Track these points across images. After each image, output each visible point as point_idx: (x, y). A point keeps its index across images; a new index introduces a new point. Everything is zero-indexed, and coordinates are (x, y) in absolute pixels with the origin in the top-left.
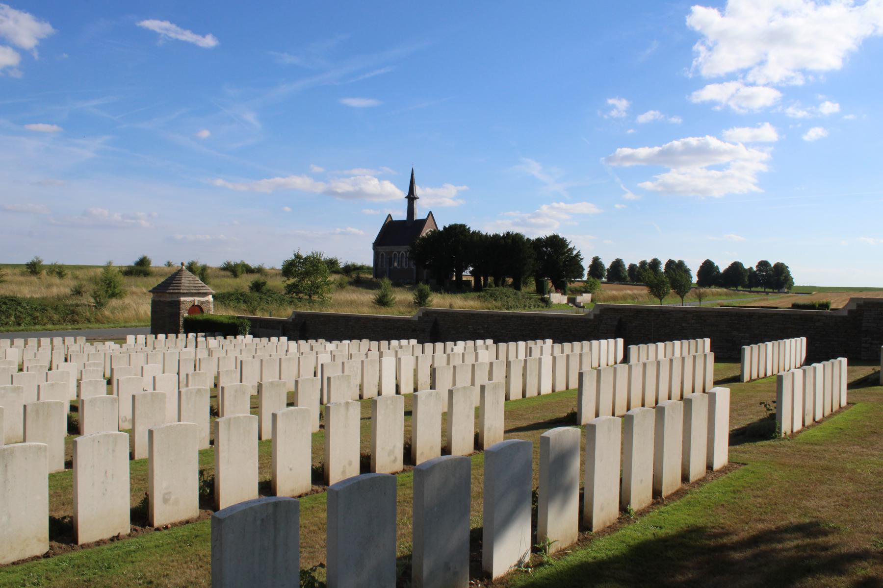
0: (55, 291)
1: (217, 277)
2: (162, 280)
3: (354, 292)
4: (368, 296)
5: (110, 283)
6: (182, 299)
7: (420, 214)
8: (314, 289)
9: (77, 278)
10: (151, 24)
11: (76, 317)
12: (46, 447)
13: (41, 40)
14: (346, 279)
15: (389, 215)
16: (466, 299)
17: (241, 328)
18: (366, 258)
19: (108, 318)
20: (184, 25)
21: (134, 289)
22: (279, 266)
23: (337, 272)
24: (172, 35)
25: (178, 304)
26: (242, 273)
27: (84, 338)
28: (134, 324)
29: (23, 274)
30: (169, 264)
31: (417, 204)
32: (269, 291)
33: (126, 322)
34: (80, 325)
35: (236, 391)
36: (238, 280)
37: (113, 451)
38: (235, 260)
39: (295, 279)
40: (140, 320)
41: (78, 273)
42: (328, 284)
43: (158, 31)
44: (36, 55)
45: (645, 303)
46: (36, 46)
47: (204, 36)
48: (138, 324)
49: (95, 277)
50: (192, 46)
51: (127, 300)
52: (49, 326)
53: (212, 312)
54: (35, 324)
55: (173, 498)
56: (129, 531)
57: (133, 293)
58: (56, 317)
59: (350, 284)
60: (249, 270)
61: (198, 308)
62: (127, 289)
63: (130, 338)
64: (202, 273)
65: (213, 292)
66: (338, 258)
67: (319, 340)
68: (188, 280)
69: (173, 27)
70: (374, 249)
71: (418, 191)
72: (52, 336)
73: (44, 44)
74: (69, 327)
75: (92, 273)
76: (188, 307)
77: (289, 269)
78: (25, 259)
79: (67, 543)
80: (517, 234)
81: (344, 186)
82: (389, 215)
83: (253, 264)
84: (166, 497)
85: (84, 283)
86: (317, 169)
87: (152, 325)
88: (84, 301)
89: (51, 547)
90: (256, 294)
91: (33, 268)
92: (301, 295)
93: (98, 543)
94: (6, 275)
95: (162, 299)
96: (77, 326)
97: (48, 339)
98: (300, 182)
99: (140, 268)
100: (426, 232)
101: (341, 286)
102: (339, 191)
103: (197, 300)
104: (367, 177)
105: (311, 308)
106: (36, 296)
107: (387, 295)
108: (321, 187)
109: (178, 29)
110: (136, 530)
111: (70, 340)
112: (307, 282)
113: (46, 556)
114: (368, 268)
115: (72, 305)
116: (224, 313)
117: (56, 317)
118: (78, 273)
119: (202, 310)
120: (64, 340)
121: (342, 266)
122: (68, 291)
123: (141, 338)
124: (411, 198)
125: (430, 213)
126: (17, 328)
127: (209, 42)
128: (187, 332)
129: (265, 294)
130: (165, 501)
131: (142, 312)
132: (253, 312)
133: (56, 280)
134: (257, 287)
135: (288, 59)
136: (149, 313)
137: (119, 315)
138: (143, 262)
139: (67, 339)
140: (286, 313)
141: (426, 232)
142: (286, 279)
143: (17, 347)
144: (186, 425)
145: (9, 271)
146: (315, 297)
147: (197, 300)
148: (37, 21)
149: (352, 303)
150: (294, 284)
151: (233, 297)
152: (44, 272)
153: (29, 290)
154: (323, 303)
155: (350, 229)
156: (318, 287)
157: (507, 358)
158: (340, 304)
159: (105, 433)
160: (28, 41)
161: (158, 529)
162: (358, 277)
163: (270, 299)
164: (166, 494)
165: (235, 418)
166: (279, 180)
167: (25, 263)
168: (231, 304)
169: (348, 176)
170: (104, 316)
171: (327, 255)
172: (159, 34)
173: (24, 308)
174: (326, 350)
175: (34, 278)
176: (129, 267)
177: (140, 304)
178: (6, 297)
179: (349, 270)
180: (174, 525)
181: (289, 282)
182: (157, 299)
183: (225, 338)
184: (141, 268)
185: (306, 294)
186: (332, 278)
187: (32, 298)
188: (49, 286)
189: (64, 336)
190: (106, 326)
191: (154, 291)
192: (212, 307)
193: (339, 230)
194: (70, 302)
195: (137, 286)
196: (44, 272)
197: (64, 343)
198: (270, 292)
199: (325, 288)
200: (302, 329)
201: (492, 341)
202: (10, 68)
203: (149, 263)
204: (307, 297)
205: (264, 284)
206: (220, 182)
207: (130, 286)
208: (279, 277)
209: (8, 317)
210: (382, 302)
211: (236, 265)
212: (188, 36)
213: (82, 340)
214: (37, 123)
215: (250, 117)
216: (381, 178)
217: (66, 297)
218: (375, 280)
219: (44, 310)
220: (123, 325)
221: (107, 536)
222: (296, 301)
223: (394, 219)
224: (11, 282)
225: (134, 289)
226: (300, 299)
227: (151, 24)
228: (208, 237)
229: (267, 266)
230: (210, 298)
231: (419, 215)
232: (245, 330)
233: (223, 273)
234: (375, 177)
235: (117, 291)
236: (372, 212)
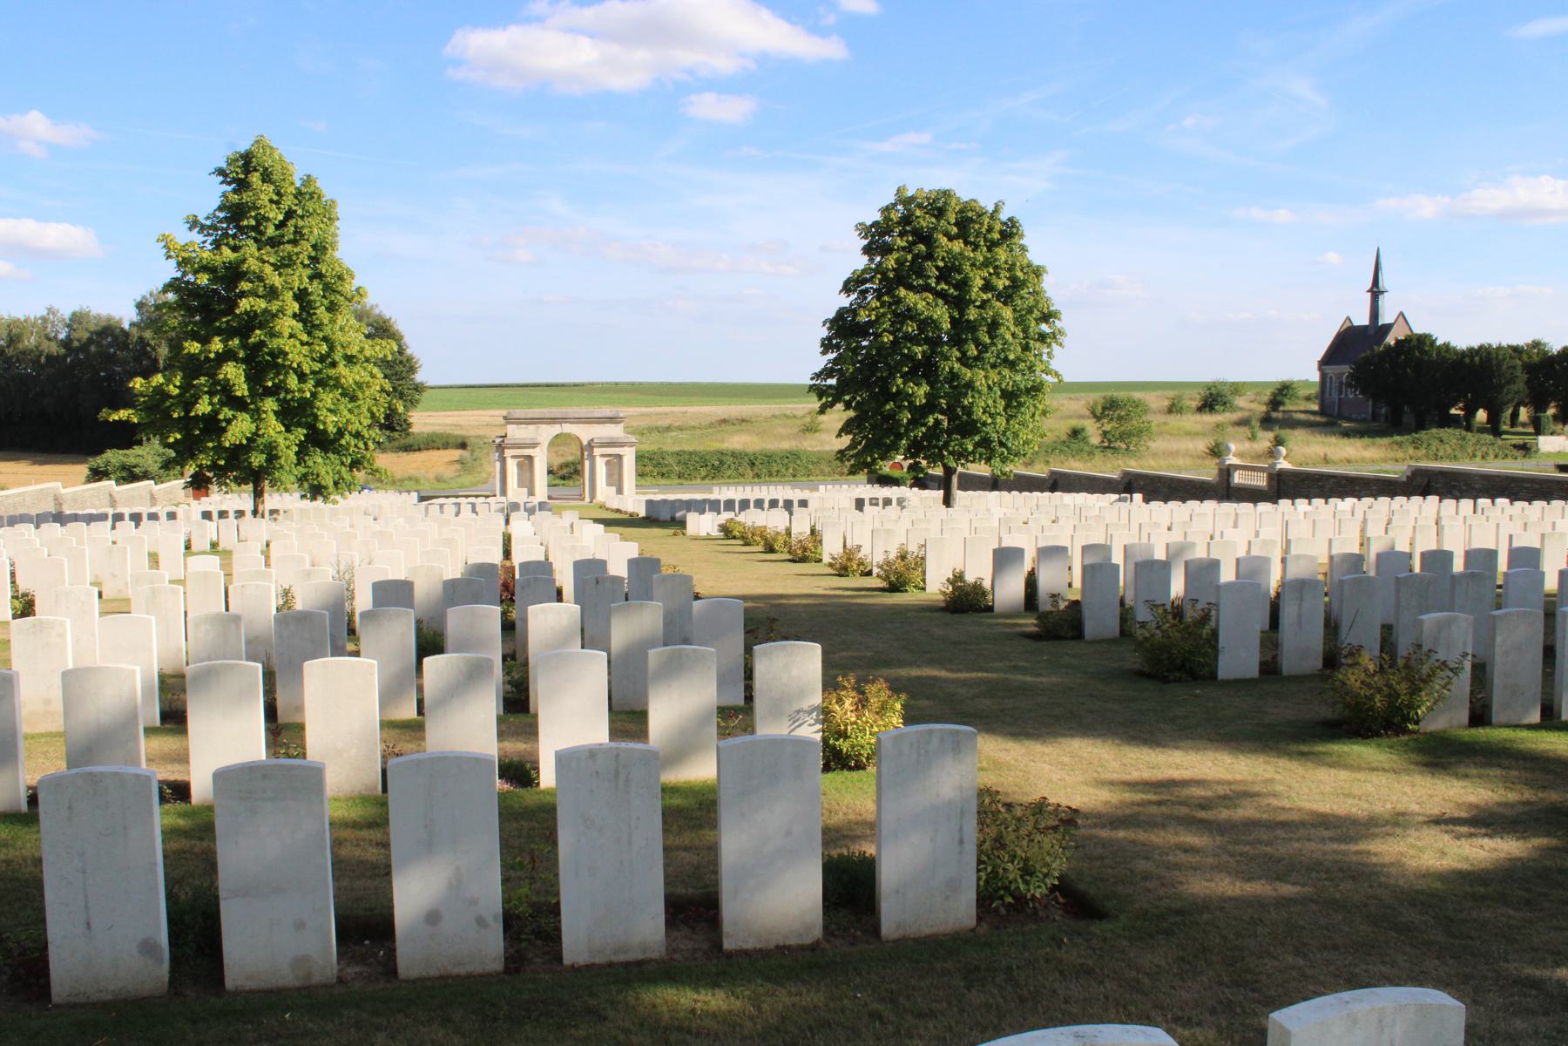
7: (1386, 318)
15: (1348, 319)
16: (1366, 447)
31: (1384, 301)
45: (1186, 469)
58: (827, 470)
71: (1385, 282)
80: (1481, 347)
82: (1348, 319)
100: (1390, 340)
124: (1376, 292)
125: (1402, 314)
141: (1390, 340)
157: (1363, 530)
174: (1069, 498)
231: (1386, 318)
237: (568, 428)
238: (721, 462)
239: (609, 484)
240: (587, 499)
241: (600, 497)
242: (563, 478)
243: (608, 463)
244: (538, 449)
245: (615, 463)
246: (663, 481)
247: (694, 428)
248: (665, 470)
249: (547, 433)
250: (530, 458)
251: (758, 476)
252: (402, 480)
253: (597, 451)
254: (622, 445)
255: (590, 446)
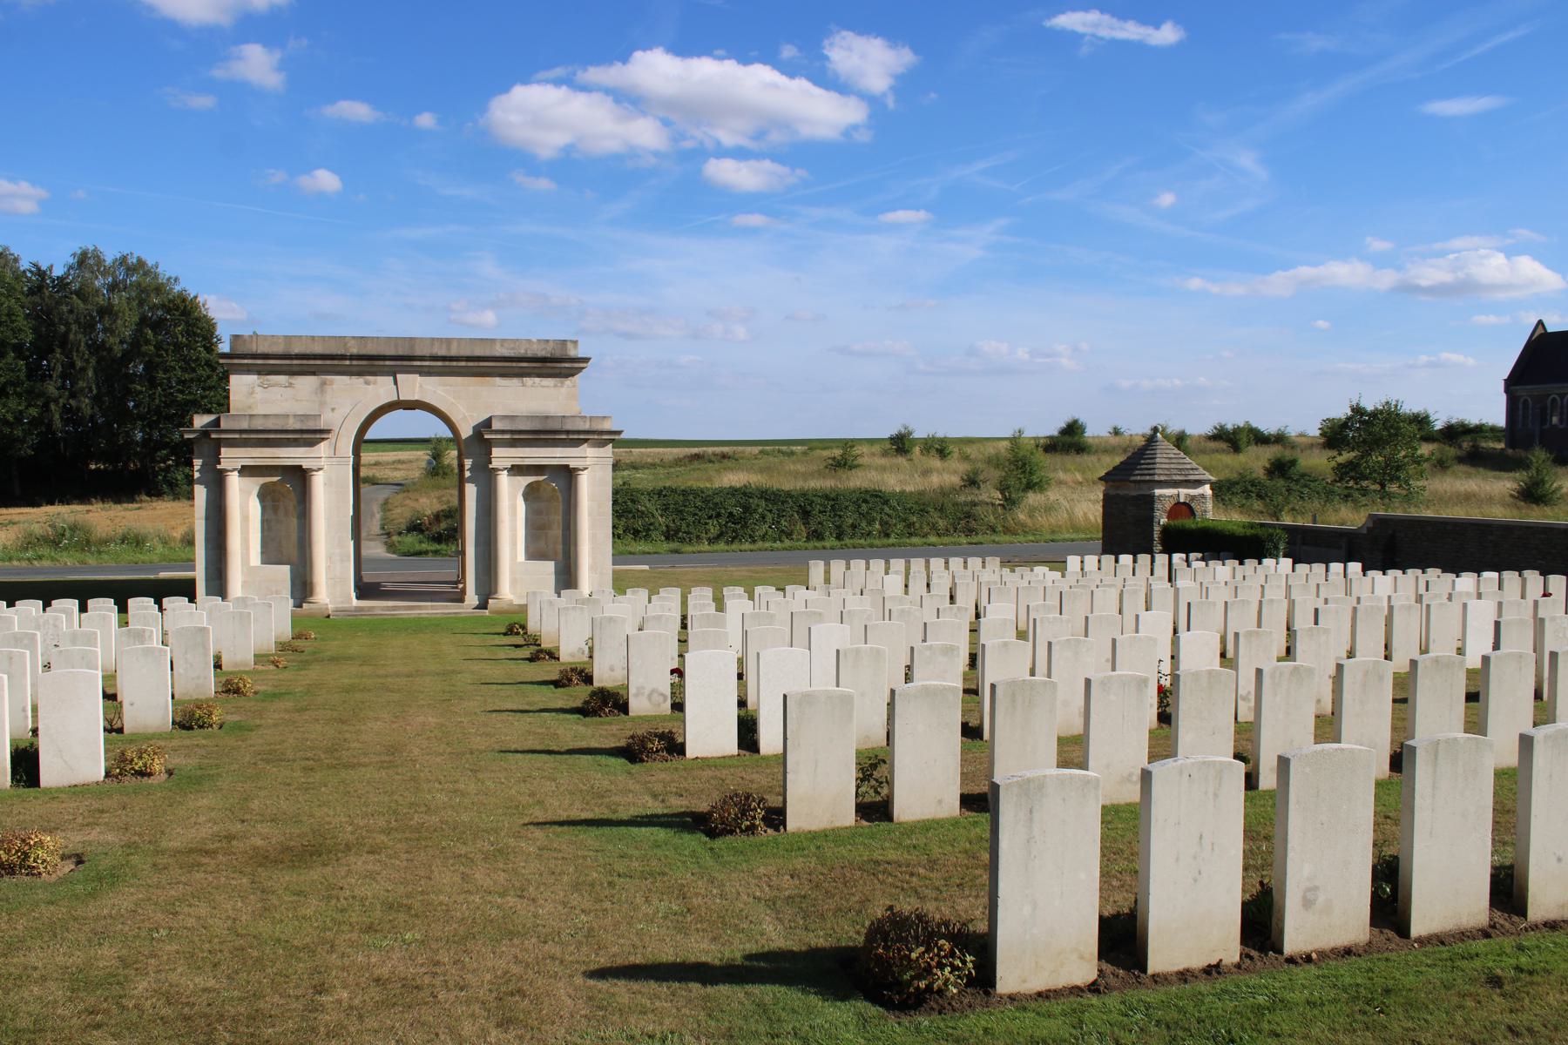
0: (936, 480)
1: (1203, 452)
2: (1118, 460)
3: (1468, 476)
4: (1503, 485)
5: (1020, 468)
6: (1158, 492)
8: (1392, 471)
9: (966, 458)
10: (1069, 21)
11: (973, 524)
12: (1097, 780)
13: (897, 77)
14: (1451, 451)
15: (1540, 323)
17: (1270, 545)
18: (1491, 410)
19: (1023, 525)
20: (1122, 15)
21: (1061, 475)
22: (1314, 431)
23: (1429, 438)
24: (1104, 33)
25: (1150, 501)
26: (1249, 443)
27: (998, 559)
28: (1067, 536)
29: (885, 454)
30: (1116, 432)
32: (1303, 475)
33: (1053, 532)
34: (980, 538)
35: (1366, 673)
36: (1242, 458)
37: (1216, 795)
38: (1232, 421)
39: (1353, 454)
40: (1076, 529)
41: (968, 450)
42: (1418, 461)
43: (1080, 29)
44: (890, 102)
45: (74, 570)
46: (892, 88)
47: (1157, 27)
48: (1074, 536)
49: (997, 456)
50: (1139, 48)
51: (1053, 495)
52: (933, 539)
53: (1210, 516)
54: (911, 535)
55: (1321, 898)
56: (1237, 958)
57: (1060, 483)
58: (942, 524)
59: (1461, 460)
60: (1261, 439)
61: (1183, 509)
62: (1051, 475)
63: (1073, 562)
64: (1180, 440)
65: (1213, 479)
66: (1431, 412)
67: (1390, 572)
68: (1165, 455)
69: (1106, 18)
70: (1507, 390)
72: (927, 557)
73: (904, 84)
74: (964, 540)
75: (990, 450)
76: (1168, 506)
77: (1335, 435)
78: (886, 430)
79: (1128, 969)
81: (1432, 274)
82: (1540, 323)
83: (1268, 426)
84: (1310, 896)
85: (980, 465)
86: (1379, 245)
87: (1104, 538)
88: (984, 497)
89: (1100, 971)
90: (1281, 482)
91: (900, 444)
92: (1365, 483)
93: (1184, 976)
94: (861, 456)
95: (1121, 492)
96: (975, 539)
97: (922, 561)
98: (1345, 273)
99: (1068, 439)
101: (1441, 465)
102: (1424, 283)
103: (1184, 493)
104: (1482, 252)
105: (1387, 508)
106: (909, 488)
107: (1543, 482)
108: (1387, 279)
109: (1114, 20)
110: (1251, 958)
111: (956, 562)
112: (1377, 458)
113: (1094, 988)
114: (1493, 429)
115: (966, 504)
116: (1233, 518)
117: (942, 524)
118: (968, 450)
119: (1192, 512)
120: (947, 563)
121: (1438, 426)
122: (955, 480)
123: (1091, 560)
126: (886, 541)
127: (1167, 35)
128: (1169, 550)
129: (1297, 481)
130: (1307, 903)
131: (1080, 515)
132: (1275, 515)
133: (936, 463)
134: (1280, 468)
135: (1316, 43)
136: (1100, 521)
137: (1041, 520)
138: (1073, 429)
139: (933, 561)
140: (1350, 517)
142: (1335, 453)
143: (896, 573)
144: (1352, 751)
145: (865, 449)
146: (1393, 488)
147: (1184, 493)
148: (891, 47)
149: (1468, 498)
150: (1350, 463)
151: (1237, 489)
152: (917, 450)
153: (896, 479)
154: (1408, 498)
155: (1445, 355)
156: (1398, 468)
158: (1443, 500)
159: (1200, 758)
160: (878, 83)
161: (1291, 960)
162: (1475, 447)
163: (1306, 490)
164: (1308, 890)
165: (1447, 741)
166: (1305, 271)
167: (887, 436)
168: (1235, 500)
169: (1442, 254)
170: (1019, 523)
171: (1410, 406)
172: (1082, 36)
173: (894, 509)
175: (901, 460)
176: (1051, 438)
177: (1080, 502)
178: (867, 491)
179: (1454, 433)
180: (1323, 955)
181: (1340, 459)
182: (1112, 492)
183: (1241, 563)
184: (1070, 440)
185: (1375, 482)
186: (1425, 449)
187: (903, 492)
188: (926, 473)
189: (946, 556)
190: (1021, 538)
191: (1105, 479)
192: (1209, 505)
193: (1423, 359)
194: (962, 499)
195: (1066, 470)
196: (917, 450)
197: (947, 568)
198: (1307, 479)
199: (1412, 469)
200: (1388, 547)
201: (1359, 565)
202: (855, 127)
203: (1083, 431)
204: (1377, 487)
205: (1293, 462)
206: (1195, 283)
207: (1055, 470)
208: (1316, 451)
209: (870, 523)
210: (1532, 494)
211: (1237, 430)
212: (1131, 31)
213: (994, 562)
214: (894, 210)
215: (1247, 160)
216: (1510, 253)
217: (953, 490)
218: (1510, 451)
219: (923, 512)
220: (1049, 537)
221: (1198, 962)
222: (1356, 495)
223: (1551, 328)
224: (869, 467)
225: (1061, 475)
226: (1364, 492)
227: (1069, 21)
228: (1177, 382)
229: (1292, 432)
230: (1207, 490)
232: (1276, 548)
233: (1213, 445)
234: (1500, 250)
235: (1035, 479)
236: (1492, 319)
237: (414, 386)
238: (746, 509)
239: (534, 554)
240: (472, 598)
241: (508, 592)
242: (438, 539)
243: (530, 494)
244: (323, 448)
245: (553, 495)
246: (642, 546)
247: (653, 465)
248: (639, 524)
249: (346, 401)
250: (300, 477)
251: (817, 535)
252: (105, 542)
253: (502, 457)
254: (574, 438)
255: (482, 440)
